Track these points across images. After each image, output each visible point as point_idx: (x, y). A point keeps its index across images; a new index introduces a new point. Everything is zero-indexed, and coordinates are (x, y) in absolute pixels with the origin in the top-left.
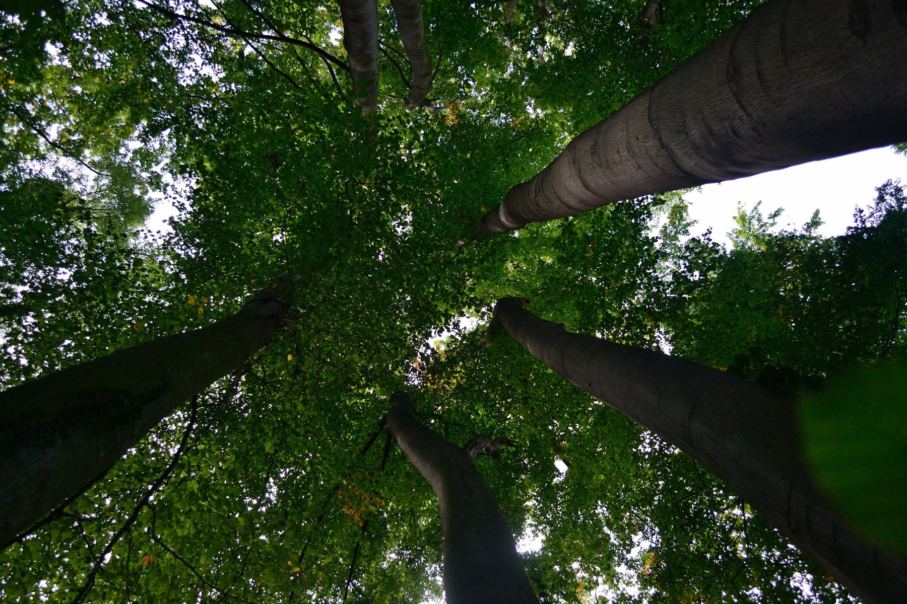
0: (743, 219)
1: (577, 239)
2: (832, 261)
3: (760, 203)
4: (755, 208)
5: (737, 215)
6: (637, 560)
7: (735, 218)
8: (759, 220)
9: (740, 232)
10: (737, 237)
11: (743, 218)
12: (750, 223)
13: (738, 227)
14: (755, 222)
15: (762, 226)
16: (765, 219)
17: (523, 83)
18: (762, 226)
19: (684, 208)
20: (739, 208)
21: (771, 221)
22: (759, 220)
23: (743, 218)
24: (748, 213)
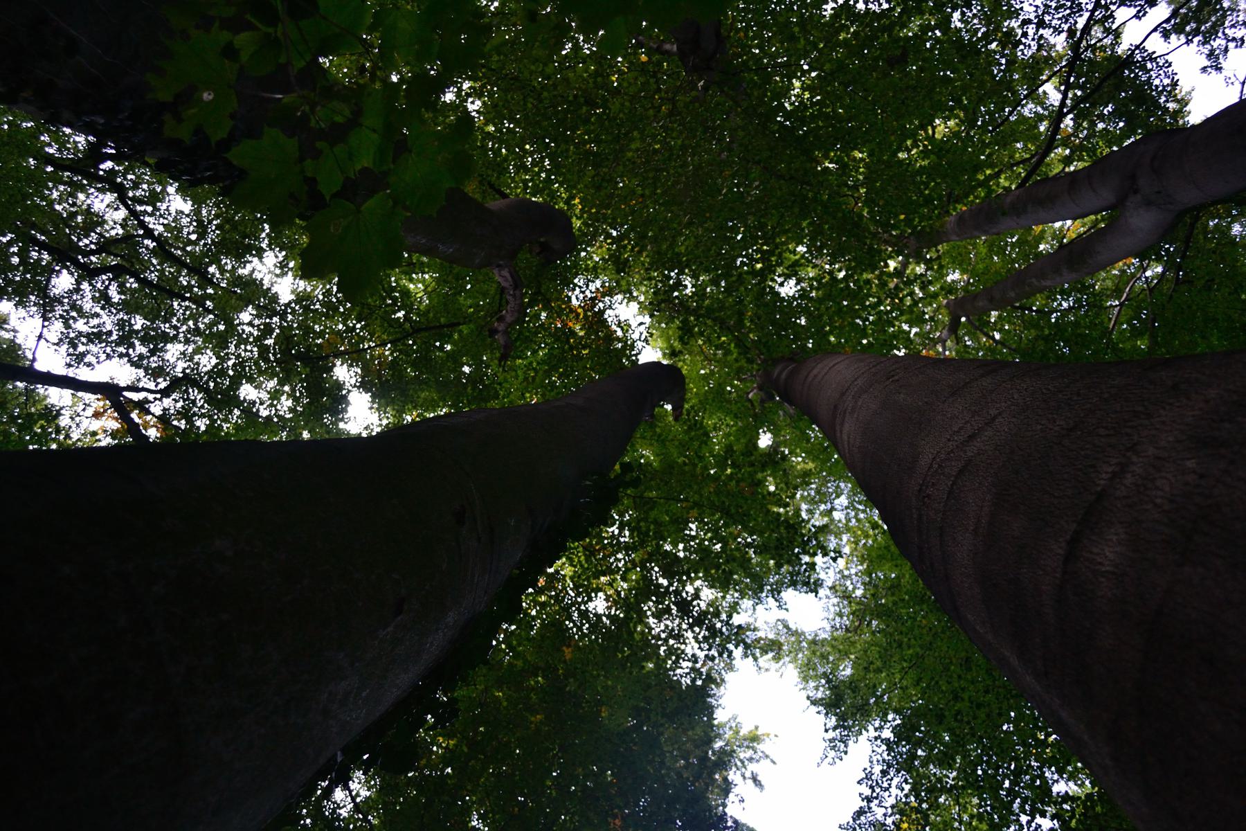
0: (754, 738)
1: (756, 473)
2: (37, 439)
3: (819, 765)
4: (767, 756)
5: (759, 733)
6: (498, 178)
7: (757, 728)
8: (751, 759)
9: (737, 732)
10: (731, 728)
11: (754, 738)
12: (748, 747)
13: (744, 732)
14: (749, 753)
15: (742, 762)
16: (752, 767)
17: (1213, 19)
18: (742, 762)
19: (777, 658)
20: (768, 735)
21: (748, 774)
22: (751, 759)
23: (754, 738)
24: (760, 747)
